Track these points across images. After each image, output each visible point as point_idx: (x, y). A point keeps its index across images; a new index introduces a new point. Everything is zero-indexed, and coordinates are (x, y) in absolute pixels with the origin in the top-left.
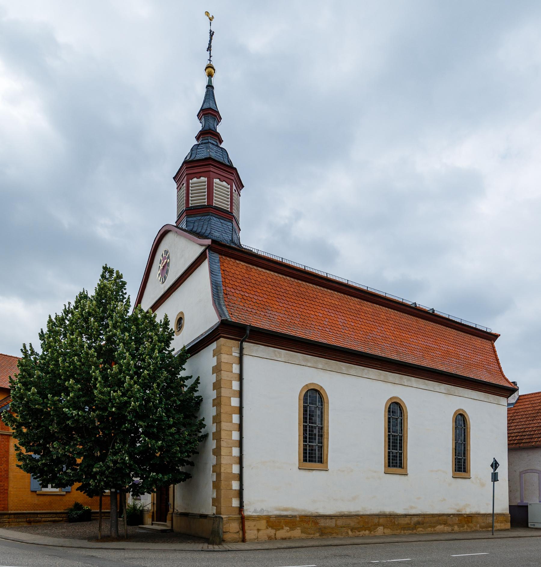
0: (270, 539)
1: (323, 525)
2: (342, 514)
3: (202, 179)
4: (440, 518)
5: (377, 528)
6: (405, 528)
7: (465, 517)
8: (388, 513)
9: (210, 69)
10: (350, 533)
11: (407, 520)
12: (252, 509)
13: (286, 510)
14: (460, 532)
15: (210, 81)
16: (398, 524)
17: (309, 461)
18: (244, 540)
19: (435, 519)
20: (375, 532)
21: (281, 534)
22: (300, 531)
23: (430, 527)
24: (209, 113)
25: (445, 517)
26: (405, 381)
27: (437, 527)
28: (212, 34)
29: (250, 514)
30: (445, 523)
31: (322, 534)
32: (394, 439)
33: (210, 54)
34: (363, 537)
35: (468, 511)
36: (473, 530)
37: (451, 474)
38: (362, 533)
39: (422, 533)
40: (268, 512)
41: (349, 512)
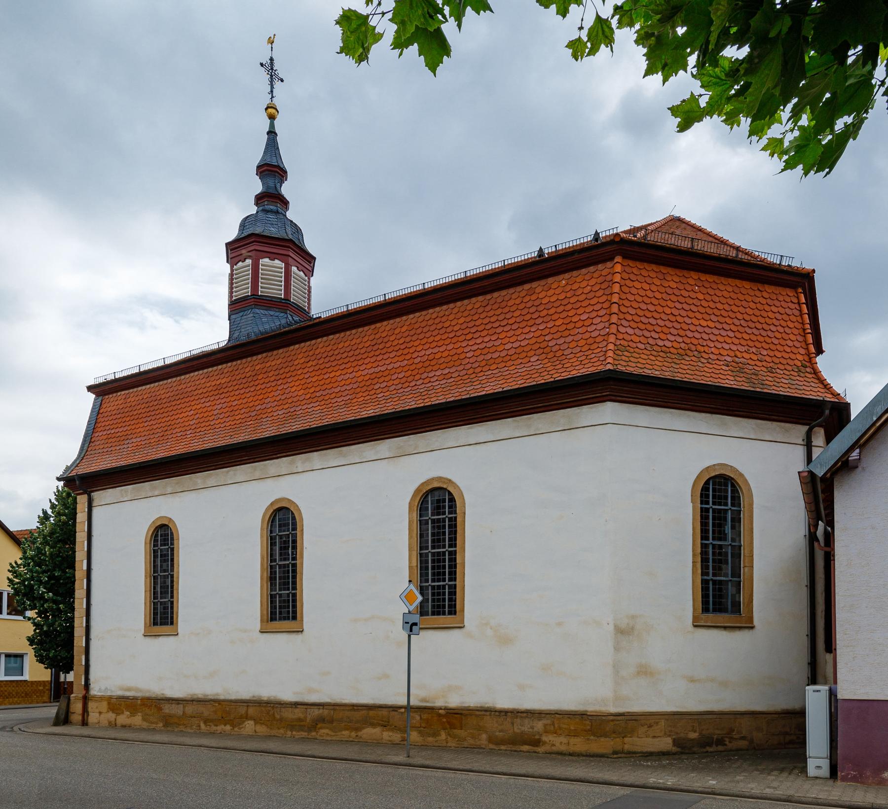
0: (113, 725)
1: (167, 711)
2: (195, 697)
4: (371, 713)
5: (244, 722)
6: (294, 725)
7: (440, 715)
8: (265, 699)
9: (270, 110)
10: (203, 726)
11: (298, 713)
12: (97, 688)
13: (129, 689)
14: (424, 747)
15: (272, 125)
16: (281, 720)
18: (84, 723)
19: (358, 715)
20: (240, 729)
21: (123, 719)
22: (140, 718)
23: (347, 729)
24: (272, 170)
25: (385, 712)
26: (199, 481)
27: (365, 731)
29: (95, 693)
30: (385, 725)
31: (166, 725)
32: (284, 572)
34: (222, 735)
35: (454, 701)
36: (466, 744)
38: (220, 728)
39: (329, 738)
40: (112, 691)
41: (205, 695)
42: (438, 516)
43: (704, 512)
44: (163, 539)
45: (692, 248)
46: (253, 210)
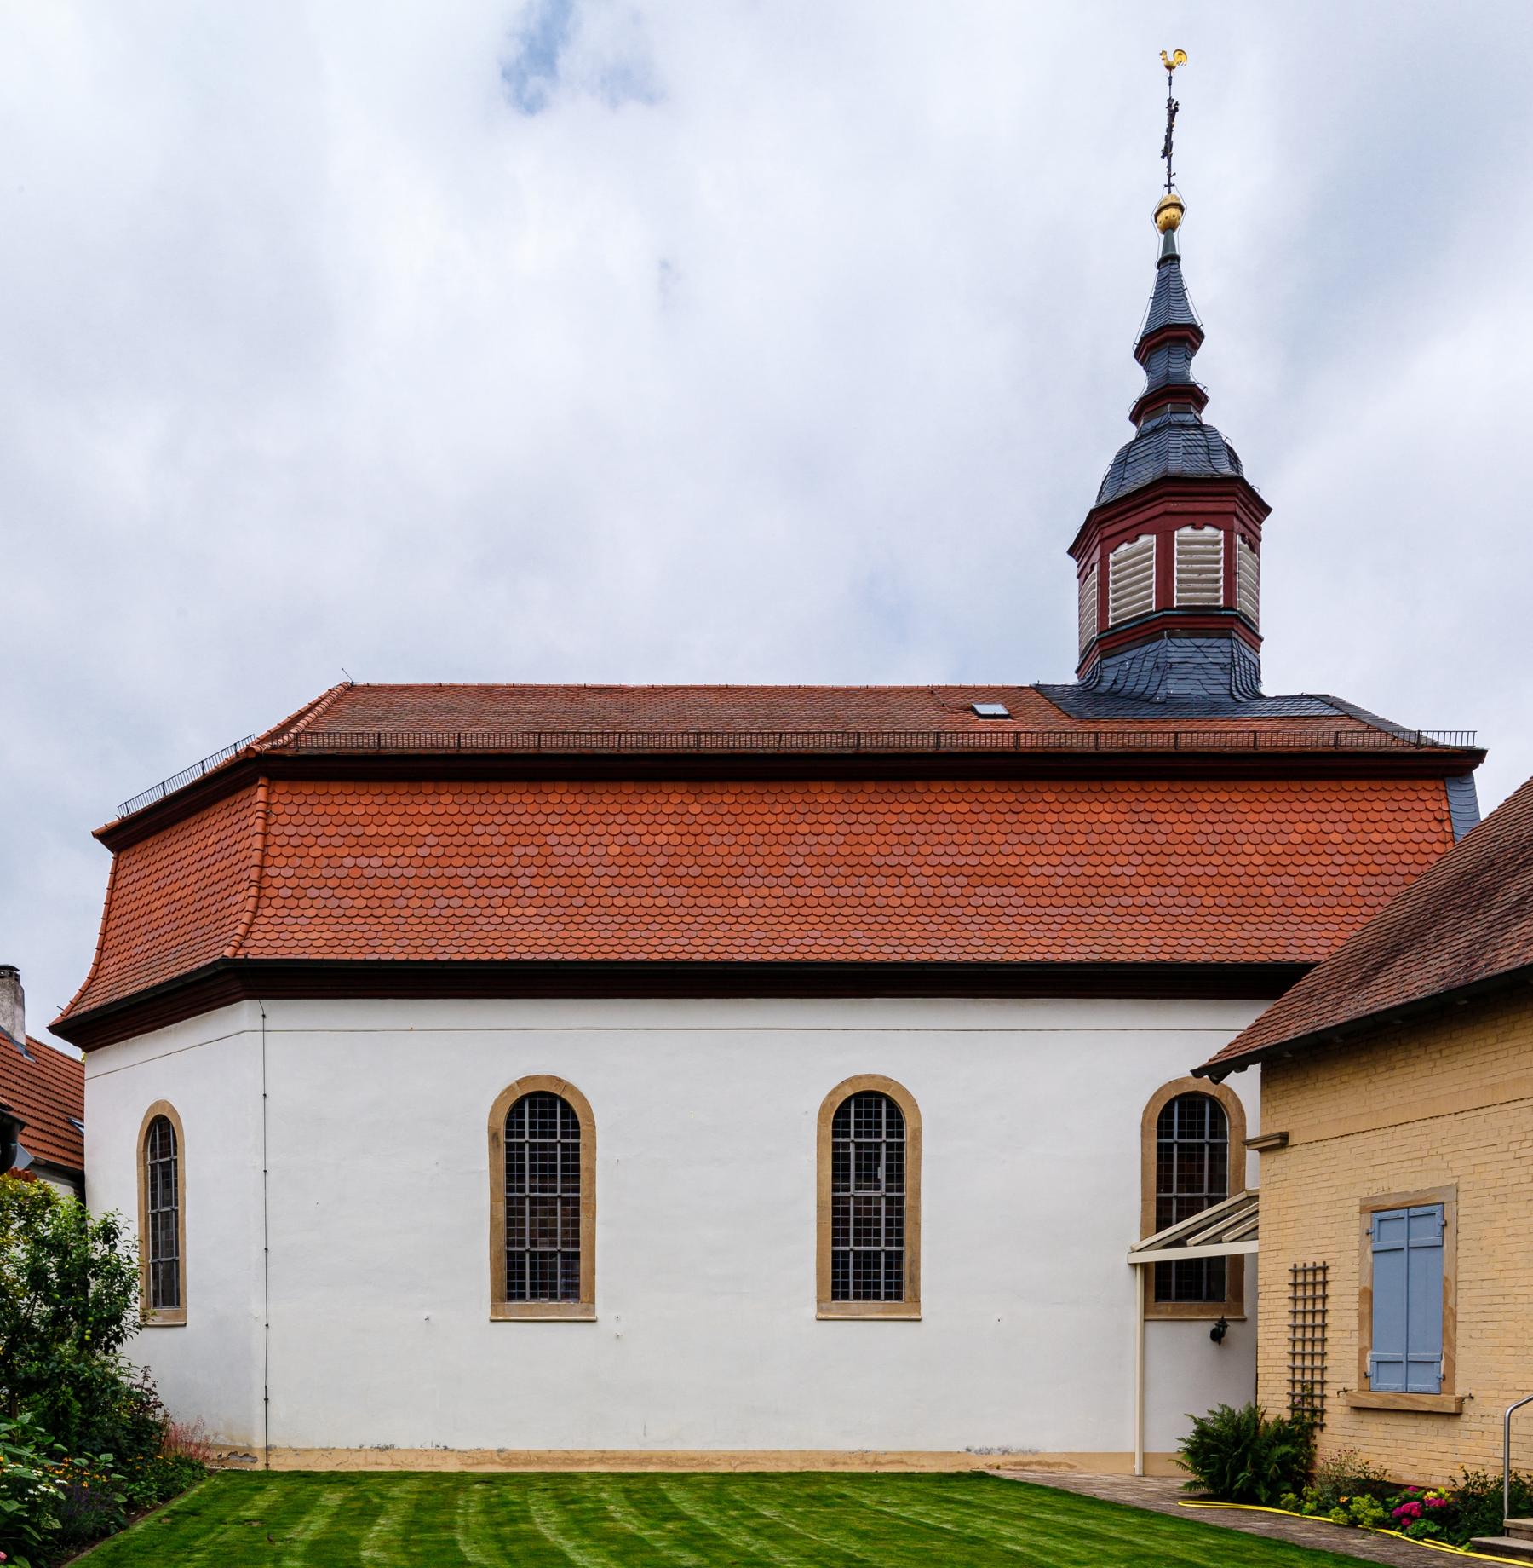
3: (1143, 539)
9: (1173, 211)
15: (1169, 244)
17: (857, 1296)
24: (1170, 337)
28: (1173, 110)
33: (1169, 166)
37: (811, 1310)
42: (869, 1136)
43: (1164, 1152)
44: (161, 1135)
45: (937, 746)
46: (1131, 432)
